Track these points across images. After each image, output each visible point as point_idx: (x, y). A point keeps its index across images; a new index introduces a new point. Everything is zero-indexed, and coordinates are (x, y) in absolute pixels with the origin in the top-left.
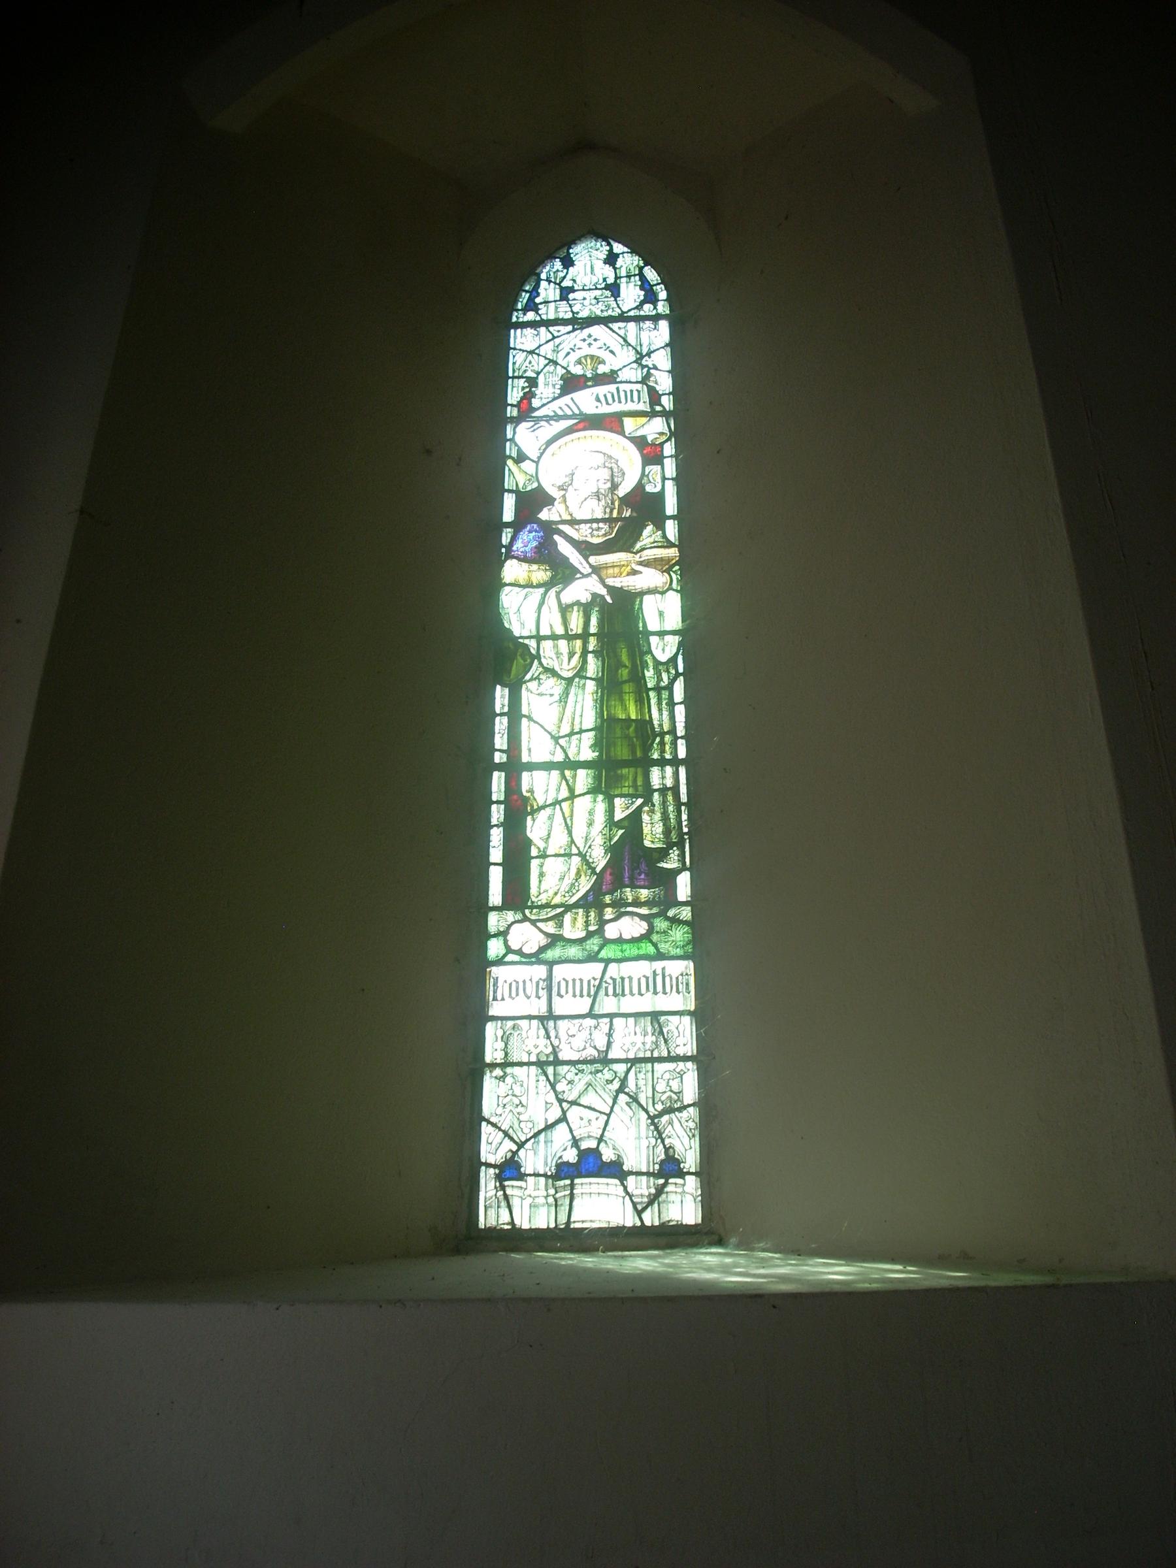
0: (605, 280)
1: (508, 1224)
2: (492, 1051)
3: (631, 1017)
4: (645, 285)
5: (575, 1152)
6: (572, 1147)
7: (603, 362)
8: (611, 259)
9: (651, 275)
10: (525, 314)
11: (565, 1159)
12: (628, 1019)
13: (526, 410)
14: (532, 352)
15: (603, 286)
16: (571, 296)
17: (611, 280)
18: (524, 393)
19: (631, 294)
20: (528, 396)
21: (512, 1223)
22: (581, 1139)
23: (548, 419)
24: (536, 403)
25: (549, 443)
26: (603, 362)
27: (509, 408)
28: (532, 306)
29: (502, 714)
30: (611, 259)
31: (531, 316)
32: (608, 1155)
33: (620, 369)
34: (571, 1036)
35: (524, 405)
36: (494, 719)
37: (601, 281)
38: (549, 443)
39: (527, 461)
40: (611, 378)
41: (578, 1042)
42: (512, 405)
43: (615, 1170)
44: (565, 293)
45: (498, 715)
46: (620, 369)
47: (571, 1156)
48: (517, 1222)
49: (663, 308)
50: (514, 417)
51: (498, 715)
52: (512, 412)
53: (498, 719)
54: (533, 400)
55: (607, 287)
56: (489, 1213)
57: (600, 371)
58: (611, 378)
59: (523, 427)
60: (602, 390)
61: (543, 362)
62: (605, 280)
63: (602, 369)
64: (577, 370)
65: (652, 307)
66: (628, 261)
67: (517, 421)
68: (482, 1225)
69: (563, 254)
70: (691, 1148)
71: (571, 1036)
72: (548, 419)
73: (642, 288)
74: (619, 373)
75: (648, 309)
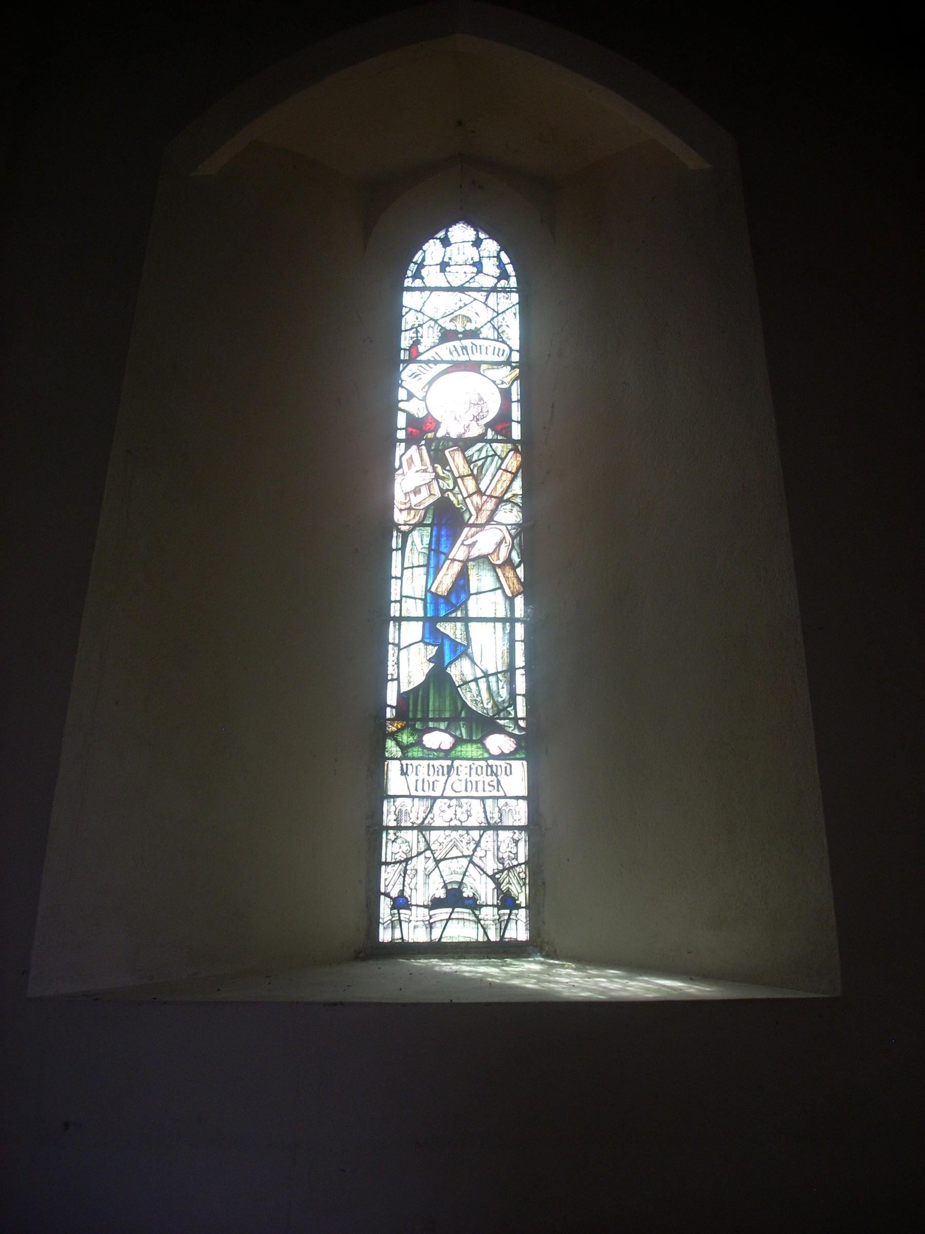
0: (472, 259)
1: (400, 939)
2: (389, 820)
3: (500, 622)
4: (501, 266)
5: (444, 891)
6: (442, 888)
7: (470, 321)
8: (477, 243)
9: (505, 258)
10: (413, 281)
11: (437, 896)
12: (496, 623)
13: (414, 356)
14: (407, 860)
15: (471, 262)
16: (448, 269)
17: (476, 259)
18: (413, 341)
19: (490, 267)
20: (416, 343)
21: (402, 938)
22: (483, 257)
23: (427, 362)
24: (421, 349)
25: (430, 383)
26: (470, 321)
27: (402, 352)
28: (417, 275)
29: (397, 550)
30: (477, 243)
31: (418, 283)
32: (467, 893)
33: (482, 327)
34: (442, 811)
35: (413, 351)
36: (392, 554)
37: (470, 259)
38: (430, 383)
39: (415, 398)
40: (474, 334)
41: (450, 814)
42: (405, 350)
43: (473, 904)
44: (444, 266)
45: (394, 550)
46: (482, 327)
47: (441, 894)
48: (405, 938)
49: (513, 282)
50: (407, 360)
51: (394, 550)
52: (403, 355)
53: (394, 553)
54: (419, 346)
55: (474, 264)
56: (388, 845)
57: (467, 328)
58: (474, 334)
59: (413, 367)
60: (467, 343)
61: (426, 319)
62: (472, 259)
63: (469, 327)
64: (450, 326)
65: (506, 282)
66: (490, 246)
67: (408, 362)
68: (381, 940)
69: (441, 234)
70: (522, 892)
71: (442, 811)
72: (427, 362)
73: (498, 267)
74: (481, 329)
75: (503, 283)
